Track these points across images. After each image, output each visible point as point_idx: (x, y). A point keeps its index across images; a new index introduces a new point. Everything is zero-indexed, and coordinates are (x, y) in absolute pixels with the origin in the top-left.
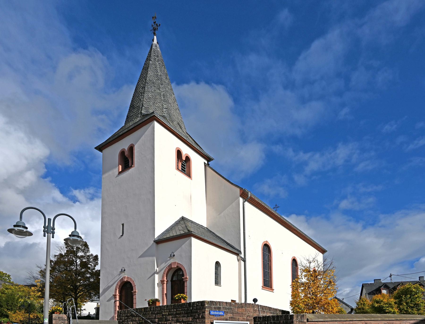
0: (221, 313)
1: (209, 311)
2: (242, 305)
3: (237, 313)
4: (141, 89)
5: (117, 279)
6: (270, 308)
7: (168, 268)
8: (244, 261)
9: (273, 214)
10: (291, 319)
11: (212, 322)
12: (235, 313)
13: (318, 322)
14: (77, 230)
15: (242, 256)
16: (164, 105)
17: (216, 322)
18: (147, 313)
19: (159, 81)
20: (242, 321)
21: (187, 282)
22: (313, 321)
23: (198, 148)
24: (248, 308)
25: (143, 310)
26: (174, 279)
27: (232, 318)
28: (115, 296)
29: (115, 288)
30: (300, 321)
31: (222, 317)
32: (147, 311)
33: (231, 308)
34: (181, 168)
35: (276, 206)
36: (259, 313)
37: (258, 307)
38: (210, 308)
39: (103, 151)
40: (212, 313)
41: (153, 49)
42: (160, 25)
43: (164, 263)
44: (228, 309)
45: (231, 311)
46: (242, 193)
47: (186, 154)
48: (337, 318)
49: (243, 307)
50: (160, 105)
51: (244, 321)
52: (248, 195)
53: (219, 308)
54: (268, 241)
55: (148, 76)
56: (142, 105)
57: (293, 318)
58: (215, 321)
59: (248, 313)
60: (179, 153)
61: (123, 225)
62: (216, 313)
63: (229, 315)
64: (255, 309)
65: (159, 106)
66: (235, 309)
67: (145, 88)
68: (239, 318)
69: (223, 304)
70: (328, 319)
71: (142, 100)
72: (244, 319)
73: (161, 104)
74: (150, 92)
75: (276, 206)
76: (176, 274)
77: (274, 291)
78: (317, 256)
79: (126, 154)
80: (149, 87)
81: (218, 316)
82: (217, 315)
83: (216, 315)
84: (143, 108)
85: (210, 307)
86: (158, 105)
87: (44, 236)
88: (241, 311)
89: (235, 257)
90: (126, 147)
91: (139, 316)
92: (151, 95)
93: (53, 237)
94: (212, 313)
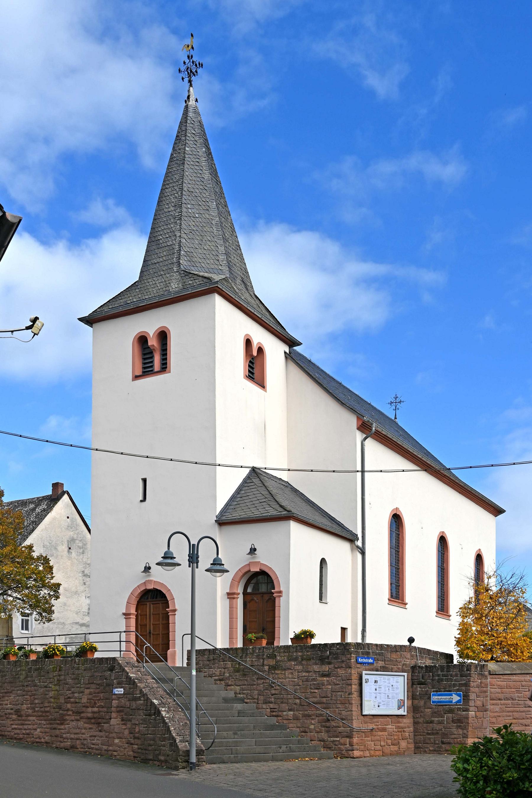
0: (371, 661)
1: (356, 657)
2: (396, 648)
3: (390, 660)
4: (172, 209)
6: (428, 652)
8: (363, 553)
9: (408, 453)
10: (467, 670)
11: (360, 673)
12: (388, 661)
13: (503, 675)
14: (220, 556)
15: (359, 543)
16: (219, 247)
17: (365, 674)
19: (207, 194)
20: (396, 672)
21: (280, 599)
22: (497, 673)
23: (278, 329)
24: (404, 653)
26: (249, 590)
27: (383, 667)
30: (479, 674)
31: (372, 667)
33: (382, 653)
34: (249, 370)
35: (396, 398)
36: (417, 660)
37: (415, 650)
38: (357, 653)
39: (94, 325)
40: (360, 660)
41: (190, 119)
44: (379, 654)
45: (383, 658)
46: (362, 424)
47: (259, 343)
48: (529, 670)
49: (398, 651)
51: (399, 672)
52: (371, 430)
53: (368, 653)
54: (399, 509)
55: (186, 181)
56: (180, 246)
57: (471, 669)
58: (364, 672)
59: (404, 660)
60: (248, 342)
61: (145, 481)
62: (365, 660)
63: (381, 664)
64: (413, 653)
65: (210, 249)
66: (387, 653)
68: (392, 668)
69: (372, 646)
70: (517, 671)
71: (178, 234)
72: (399, 668)
73: (214, 245)
74: (192, 218)
75: (396, 398)
76: (254, 581)
77: (407, 606)
78: (500, 567)
80: (189, 206)
81: (367, 665)
82: (365, 664)
83: (364, 664)
85: (357, 651)
87: (189, 566)
88: (394, 657)
89: (346, 546)
90: (151, 331)
91: (233, 661)
92: (193, 223)
93: (197, 567)
94: (359, 660)
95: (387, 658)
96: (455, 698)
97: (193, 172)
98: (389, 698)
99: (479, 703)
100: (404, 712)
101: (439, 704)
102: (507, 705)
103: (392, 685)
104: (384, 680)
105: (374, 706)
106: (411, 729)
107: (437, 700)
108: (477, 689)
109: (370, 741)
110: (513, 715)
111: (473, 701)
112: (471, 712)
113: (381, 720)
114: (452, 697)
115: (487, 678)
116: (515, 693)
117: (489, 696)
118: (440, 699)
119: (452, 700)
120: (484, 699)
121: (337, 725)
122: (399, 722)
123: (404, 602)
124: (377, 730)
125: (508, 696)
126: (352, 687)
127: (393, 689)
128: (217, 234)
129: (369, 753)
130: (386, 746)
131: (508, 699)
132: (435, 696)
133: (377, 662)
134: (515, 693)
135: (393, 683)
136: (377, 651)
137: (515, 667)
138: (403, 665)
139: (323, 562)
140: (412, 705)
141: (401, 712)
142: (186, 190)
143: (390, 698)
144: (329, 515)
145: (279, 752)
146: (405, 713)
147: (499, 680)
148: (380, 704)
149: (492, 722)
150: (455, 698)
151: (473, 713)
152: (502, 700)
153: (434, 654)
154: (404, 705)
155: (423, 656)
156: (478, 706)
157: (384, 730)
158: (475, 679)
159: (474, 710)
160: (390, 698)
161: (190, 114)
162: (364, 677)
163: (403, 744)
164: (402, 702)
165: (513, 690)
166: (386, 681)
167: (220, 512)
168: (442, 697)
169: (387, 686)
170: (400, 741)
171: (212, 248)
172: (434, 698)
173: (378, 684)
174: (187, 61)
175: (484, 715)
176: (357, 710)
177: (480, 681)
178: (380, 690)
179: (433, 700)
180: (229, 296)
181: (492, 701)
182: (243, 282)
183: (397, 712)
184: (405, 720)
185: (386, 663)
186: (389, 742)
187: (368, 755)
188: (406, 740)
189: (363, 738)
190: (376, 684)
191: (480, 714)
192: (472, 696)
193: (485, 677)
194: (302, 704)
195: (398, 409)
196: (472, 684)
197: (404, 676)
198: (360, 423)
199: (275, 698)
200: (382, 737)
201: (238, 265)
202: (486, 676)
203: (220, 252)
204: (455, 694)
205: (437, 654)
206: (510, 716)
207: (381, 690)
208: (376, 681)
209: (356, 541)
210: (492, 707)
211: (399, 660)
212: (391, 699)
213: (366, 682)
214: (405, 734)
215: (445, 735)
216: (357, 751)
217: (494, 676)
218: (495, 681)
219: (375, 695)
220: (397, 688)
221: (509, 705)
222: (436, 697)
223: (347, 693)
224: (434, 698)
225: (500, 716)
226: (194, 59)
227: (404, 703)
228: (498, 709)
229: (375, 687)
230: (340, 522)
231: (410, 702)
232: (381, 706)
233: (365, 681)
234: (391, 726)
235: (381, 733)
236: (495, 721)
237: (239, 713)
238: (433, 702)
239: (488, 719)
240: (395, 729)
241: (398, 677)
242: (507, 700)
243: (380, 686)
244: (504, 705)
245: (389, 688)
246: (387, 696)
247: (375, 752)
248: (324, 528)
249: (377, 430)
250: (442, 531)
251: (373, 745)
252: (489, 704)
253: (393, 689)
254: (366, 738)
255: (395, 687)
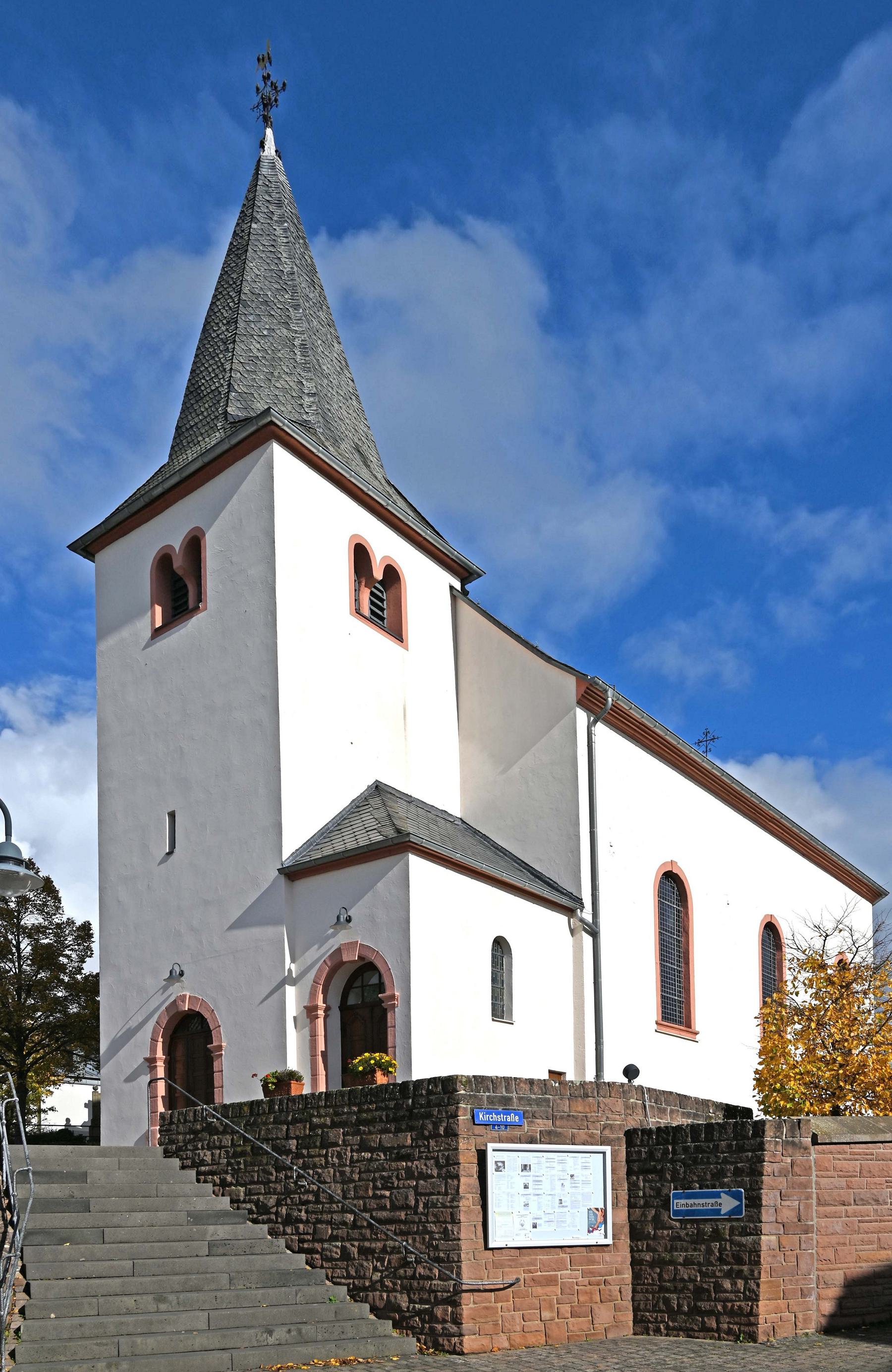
0: (513, 1118)
1: (472, 1110)
3: (569, 1116)
4: (224, 328)
5: (157, 1004)
6: (683, 1099)
7: (329, 964)
8: (594, 934)
11: (483, 1148)
12: (562, 1118)
13: (852, 1145)
14: (14, 840)
16: (305, 383)
17: (494, 1150)
18: (260, 1120)
19: (286, 297)
20: (584, 1144)
21: (394, 1012)
24: (607, 1100)
25: (246, 1109)
26: (352, 1000)
27: (549, 1133)
28: (151, 1062)
29: (150, 1036)
31: (517, 1133)
32: (261, 1112)
33: (548, 1100)
36: (646, 1116)
37: (640, 1094)
40: (481, 1117)
41: (263, 178)
42: (284, 84)
43: (316, 946)
44: (538, 1102)
45: (547, 1112)
46: (585, 692)
47: (385, 558)
49: (590, 1094)
50: (291, 384)
51: (592, 1144)
52: (606, 700)
58: (490, 1146)
59: (607, 1117)
61: (172, 815)
62: (495, 1118)
63: (542, 1125)
64: (632, 1100)
65: (287, 387)
66: (559, 1101)
67: (236, 322)
68: (573, 1135)
69: (519, 1085)
71: (228, 367)
72: (591, 1136)
73: (296, 380)
74: (255, 337)
76: (358, 983)
77: (698, 1036)
78: (849, 911)
79: (178, 563)
80: (251, 318)
81: (503, 1128)
82: (499, 1125)
84: (231, 397)
86: (283, 383)
88: (580, 1109)
89: (561, 920)
91: (234, 1132)
92: (258, 346)
94: (481, 1116)
95: (558, 1111)
96: (727, 1203)
97: (280, 288)
98: (563, 1206)
99: (788, 1215)
100: (606, 1237)
101: (689, 1218)
102: (862, 1216)
103: (572, 1176)
104: (548, 1165)
105: (522, 1225)
106: (627, 1276)
107: (683, 1208)
108: (783, 1179)
109: (509, 1311)
110: (879, 1239)
111: (772, 1210)
112: (767, 1237)
113: (542, 1257)
114: (719, 1201)
115: (810, 1153)
116: (884, 1187)
117: (814, 1196)
118: (692, 1205)
119: (718, 1207)
120: (801, 1205)
121: (428, 1273)
122: (592, 1262)
123: (690, 1030)
124: (532, 1284)
125: (864, 1193)
126: (459, 1181)
127: (573, 1185)
128: (303, 361)
129: (509, 1339)
130: (557, 1320)
131: (865, 1202)
132: (681, 1198)
133: (532, 1122)
134: (884, 1187)
135: (575, 1169)
136: (533, 1096)
137: (884, 1127)
138: (605, 1127)
139: (500, 946)
140: (629, 1221)
141: (597, 1238)
142: (248, 292)
143: (567, 1206)
144: (531, 869)
145: (265, 1343)
146: (609, 1241)
147: (839, 1156)
148: (538, 1222)
149: (822, 1258)
150: (727, 1203)
151: (774, 1238)
152: (850, 1205)
153: (697, 1106)
154: (605, 1222)
155: (665, 1110)
156: (785, 1220)
157: (551, 1281)
158: (775, 1155)
159: (774, 1231)
160: (567, 1206)
161: (264, 170)
162: (492, 1158)
163: (604, 1315)
164: (599, 1214)
165: (877, 1180)
166: (555, 1165)
167: (292, 855)
168: (697, 1201)
169: (556, 1178)
170: (594, 1306)
171: (291, 384)
172: (679, 1204)
173: (531, 1173)
174: (261, 85)
175: (802, 1242)
176: (473, 1237)
177: (789, 1160)
178: (537, 1187)
179: (675, 1208)
180: (296, 442)
181: (821, 1209)
182: (359, 451)
183: (587, 1237)
184: (607, 1257)
185: (558, 1123)
186: (566, 1309)
187: (506, 1344)
188: (612, 1304)
189: (493, 1304)
190: (525, 1173)
191: (791, 1241)
192: (768, 1197)
193: (802, 1150)
194: (359, 1224)
195: (710, 751)
196: (768, 1168)
197: (604, 1153)
198: (583, 688)
199: (307, 1212)
200: (545, 1300)
201: (348, 421)
202: (806, 1149)
203: (306, 391)
204: (724, 1192)
205: (708, 1106)
206: (871, 1243)
207: (540, 1187)
208: (525, 1166)
209: (579, 910)
210: (823, 1222)
211: (592, 1116)
212: (565, 1210)
213: (498, 1169)
214: (610, 1291)
215: (699, 1293)
216: (473, 1337)
217: (828, 1146)
218: (830, 1160)
219: (523, 1200)
220: (586, 1182)
221: (868, 1216)
222: (683, 1201)
223: (449, 1196)
224: (679, 1204)
225: (844, 1244)
226: (273, 79)
227: (605, 1217)
228: (841, 1227)
229: (524, 1181)
230: (551, 880)
231: (624, 1214)
232: (540, 1225)
233: (494, 1167)
234: (569, 1272)
235: (539, 1290)
236: (832, 1258)
237: (210, 1246)
238: (677, 1213)
239: (814, 1251)
240: (581, 1279)
241: (588, 1155)
242: (863, 1205)
243: (537, 1179)
244: (856, 1216)
245: (562, 1181)
246: (558, 1202)
247: (523, 1336)
248: (499, 877)
249: (614, 706)
250: (770, 914)
251: (519, 1320)
252: (814, 1214)
253: (573, 1185)
254: (499, 1305)
255: (579, 1177)
